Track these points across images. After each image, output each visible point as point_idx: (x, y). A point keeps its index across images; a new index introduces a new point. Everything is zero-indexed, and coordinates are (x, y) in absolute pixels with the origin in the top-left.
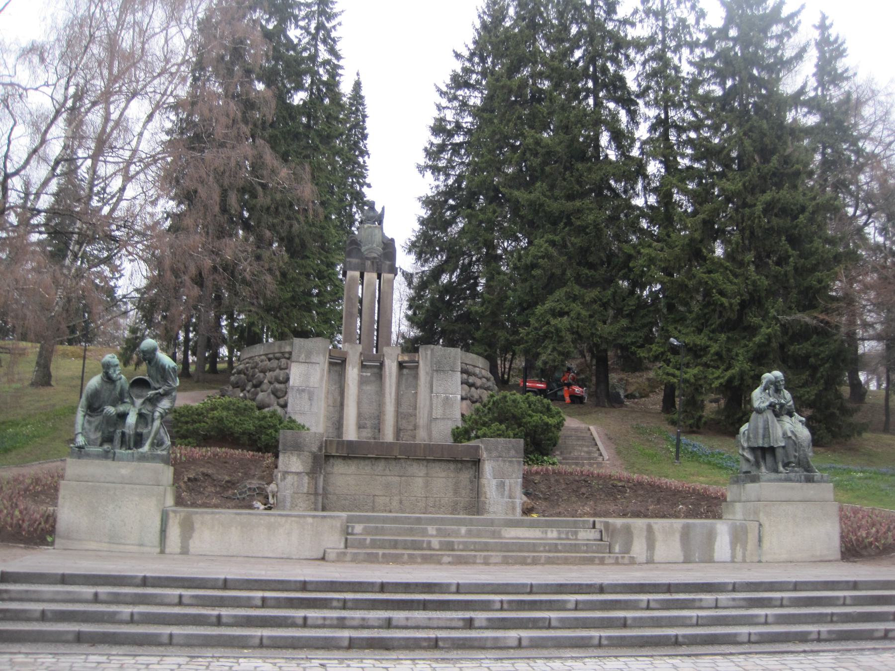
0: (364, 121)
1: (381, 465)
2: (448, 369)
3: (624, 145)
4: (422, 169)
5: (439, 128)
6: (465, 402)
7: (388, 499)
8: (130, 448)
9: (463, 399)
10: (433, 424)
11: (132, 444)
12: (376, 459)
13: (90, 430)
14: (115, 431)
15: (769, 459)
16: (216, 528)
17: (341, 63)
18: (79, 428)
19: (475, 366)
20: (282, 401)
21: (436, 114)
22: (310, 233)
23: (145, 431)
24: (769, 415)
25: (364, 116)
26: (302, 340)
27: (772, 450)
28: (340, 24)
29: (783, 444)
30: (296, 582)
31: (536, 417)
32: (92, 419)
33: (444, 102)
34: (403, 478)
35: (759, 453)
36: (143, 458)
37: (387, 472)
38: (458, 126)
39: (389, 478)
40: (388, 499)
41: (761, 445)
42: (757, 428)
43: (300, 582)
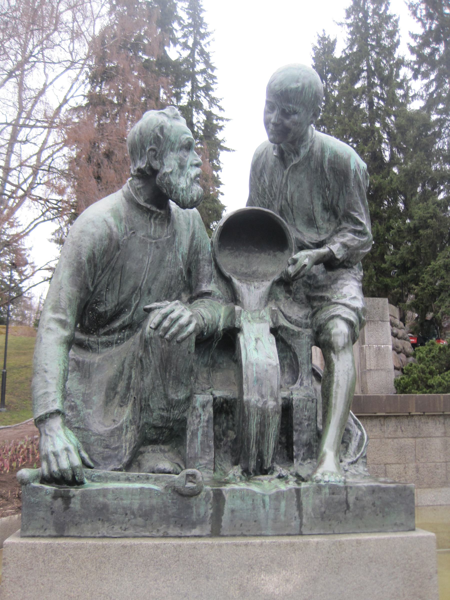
1: (391, 425)
2: (377, 319)
7: (402, 467)
10: (368, 375)
12: (385, 417)
17: (214, 74)
22: (206, 208)
28: (213, 40)
34: (418, 440)
37: (399, 433)
39: (402, 441)
40: (402, 467)
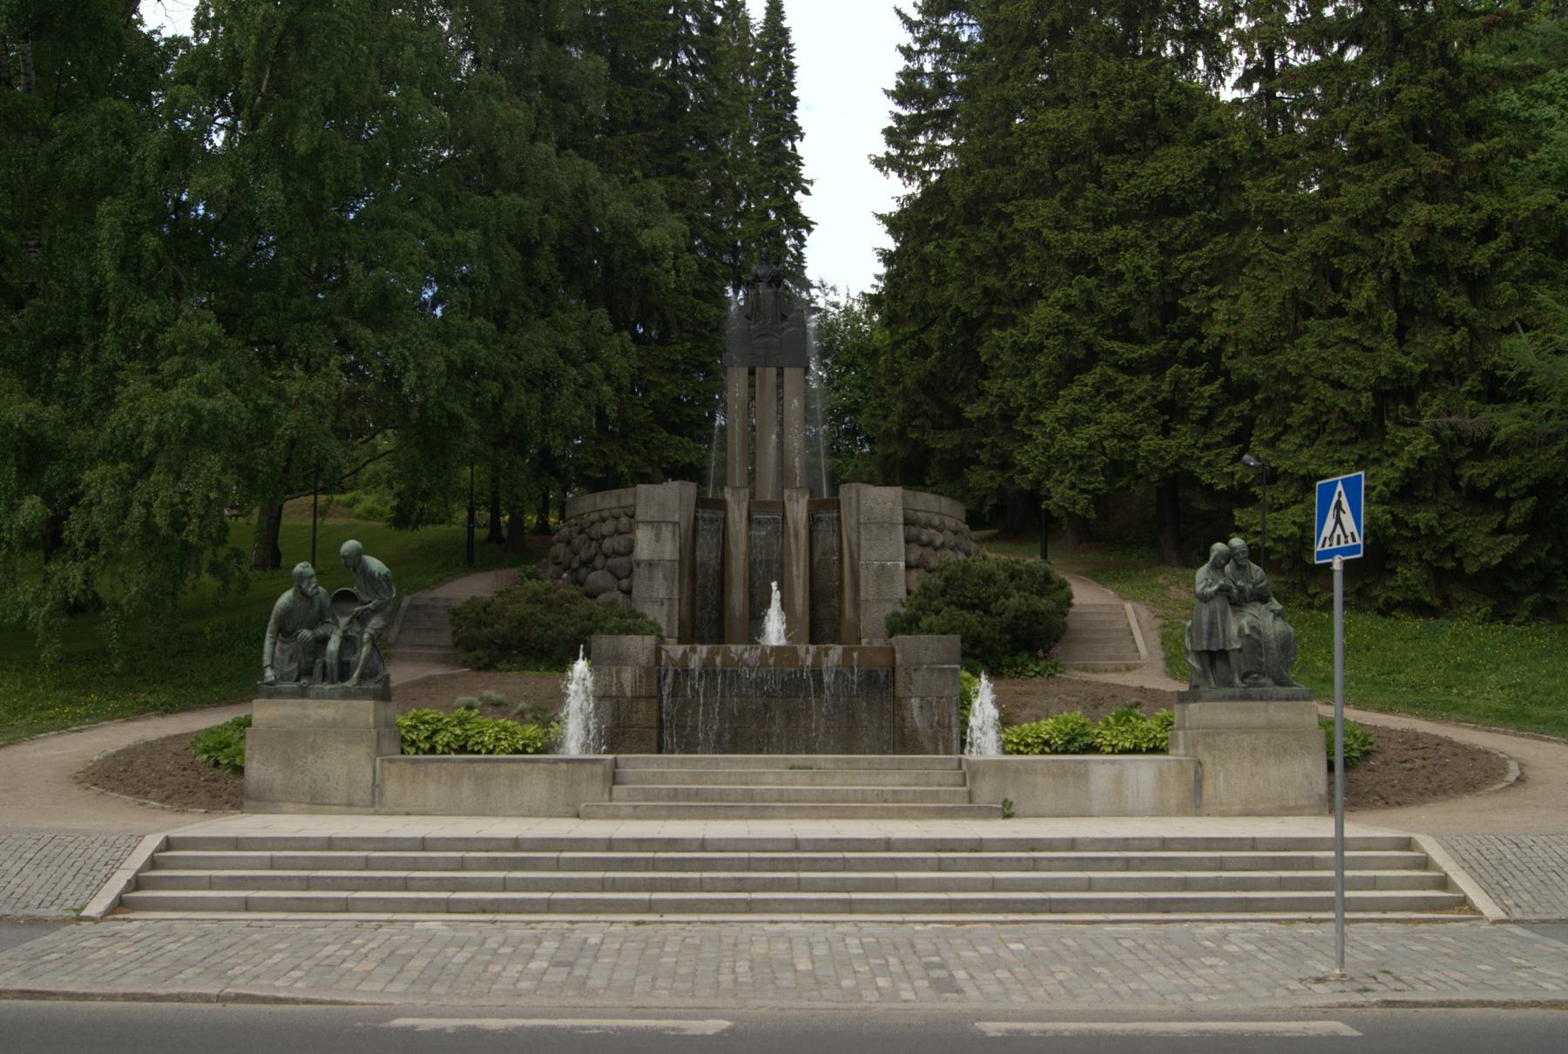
0: (791, 76)
4: (879, 163)
5: (903, 94)
6: (914, 574)
8: (333, 683)
9: (908, 567)
11: (335, 678)
13: (283, 661)
14: (314, 661)
15: (1219, 665)
18: (267, 660)
19: (916, 510)
20: (624, 583)
21: (901, 63)
23: (353, 659)
24: (1218, 604)
25: (791, 68)
26: (650, 486)
27: (1223, 654)
29: (1238, 646)
30: (507, 839)
32: (286, 646)
35: (1205, 658)
36: (347, 695)
41: (1205, 648)
42: (1200, 623)
43: (512, 839)
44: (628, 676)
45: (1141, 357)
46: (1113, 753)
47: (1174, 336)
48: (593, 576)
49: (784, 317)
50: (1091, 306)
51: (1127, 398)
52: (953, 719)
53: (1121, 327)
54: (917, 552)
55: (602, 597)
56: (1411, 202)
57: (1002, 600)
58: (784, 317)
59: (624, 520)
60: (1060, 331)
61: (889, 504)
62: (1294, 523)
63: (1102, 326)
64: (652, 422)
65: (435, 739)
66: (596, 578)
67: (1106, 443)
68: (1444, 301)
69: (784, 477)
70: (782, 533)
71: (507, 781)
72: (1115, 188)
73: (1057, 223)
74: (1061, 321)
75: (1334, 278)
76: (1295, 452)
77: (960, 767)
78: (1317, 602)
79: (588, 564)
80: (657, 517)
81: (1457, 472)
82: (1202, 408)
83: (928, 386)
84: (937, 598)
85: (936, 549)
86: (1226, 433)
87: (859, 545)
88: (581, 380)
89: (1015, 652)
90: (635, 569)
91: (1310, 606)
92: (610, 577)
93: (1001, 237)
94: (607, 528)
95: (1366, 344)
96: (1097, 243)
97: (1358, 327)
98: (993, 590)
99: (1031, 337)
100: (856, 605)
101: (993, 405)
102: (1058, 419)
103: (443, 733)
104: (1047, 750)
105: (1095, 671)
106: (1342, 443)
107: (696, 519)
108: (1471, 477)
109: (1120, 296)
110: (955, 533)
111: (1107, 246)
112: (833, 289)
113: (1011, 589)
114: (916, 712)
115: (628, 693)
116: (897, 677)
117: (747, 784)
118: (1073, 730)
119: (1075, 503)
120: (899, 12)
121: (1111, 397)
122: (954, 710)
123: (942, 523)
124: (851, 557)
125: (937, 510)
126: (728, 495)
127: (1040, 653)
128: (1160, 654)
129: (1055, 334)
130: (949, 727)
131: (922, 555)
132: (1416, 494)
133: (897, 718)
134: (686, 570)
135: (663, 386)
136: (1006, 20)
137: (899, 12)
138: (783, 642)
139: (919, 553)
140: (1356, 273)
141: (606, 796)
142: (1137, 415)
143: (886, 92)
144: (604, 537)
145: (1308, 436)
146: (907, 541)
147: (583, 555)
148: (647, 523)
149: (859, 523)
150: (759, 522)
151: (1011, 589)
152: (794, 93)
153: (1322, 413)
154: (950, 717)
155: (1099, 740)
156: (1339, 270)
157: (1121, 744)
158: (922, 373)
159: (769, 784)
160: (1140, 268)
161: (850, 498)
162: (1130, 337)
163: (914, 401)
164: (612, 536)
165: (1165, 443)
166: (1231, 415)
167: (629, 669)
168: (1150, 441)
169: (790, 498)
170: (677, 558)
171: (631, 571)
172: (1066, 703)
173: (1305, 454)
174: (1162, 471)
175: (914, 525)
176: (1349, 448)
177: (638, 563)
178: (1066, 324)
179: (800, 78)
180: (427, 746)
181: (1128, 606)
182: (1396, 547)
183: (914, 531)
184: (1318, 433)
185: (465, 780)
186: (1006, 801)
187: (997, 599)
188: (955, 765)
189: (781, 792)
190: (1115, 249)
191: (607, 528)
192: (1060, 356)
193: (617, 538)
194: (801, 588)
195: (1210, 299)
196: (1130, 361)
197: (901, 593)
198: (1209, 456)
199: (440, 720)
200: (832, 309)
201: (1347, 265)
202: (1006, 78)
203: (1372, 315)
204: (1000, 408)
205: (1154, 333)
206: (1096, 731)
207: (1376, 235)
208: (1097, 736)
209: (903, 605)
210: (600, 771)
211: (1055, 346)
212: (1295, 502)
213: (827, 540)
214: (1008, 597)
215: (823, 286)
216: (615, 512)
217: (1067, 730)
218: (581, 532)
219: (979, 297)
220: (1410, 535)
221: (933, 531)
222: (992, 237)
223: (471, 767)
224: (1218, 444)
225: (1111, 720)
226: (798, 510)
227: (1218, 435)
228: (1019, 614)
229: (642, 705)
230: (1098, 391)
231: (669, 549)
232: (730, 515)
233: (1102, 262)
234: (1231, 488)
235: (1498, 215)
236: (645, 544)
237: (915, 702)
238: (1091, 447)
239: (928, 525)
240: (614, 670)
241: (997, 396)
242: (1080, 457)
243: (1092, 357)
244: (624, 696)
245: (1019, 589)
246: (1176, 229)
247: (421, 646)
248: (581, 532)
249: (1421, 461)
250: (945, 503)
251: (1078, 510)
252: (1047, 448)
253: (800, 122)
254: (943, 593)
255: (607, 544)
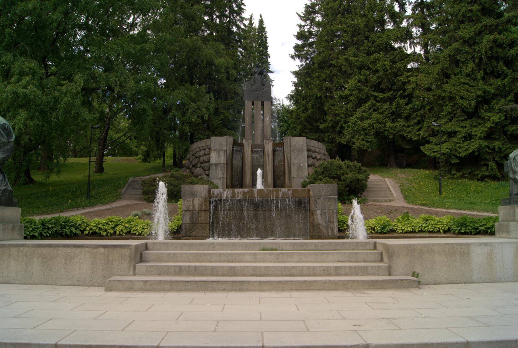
0: (266, 40)
3: (397, 21)
4: (292, 57)
5: (300, 36)
6: (310, 168)
9: (309, 166)
16: (21, 259)
19: (311, 146)
20: (207, 172)
25: (266, 38)
31: (350, 175)
33: (303, 23)
38: (310, 33)
44: (197, 202)
45: (384, 97)
46: (402, 233)
47: (395, 90)
48: (196, 170)
49: (264, 85)
50: (367, 81)
51: (380, 110)
52: (335, 219)
53: (377, 87)
54: (311, 161)
55: (199, 177)
56: (485, 35)
57: (345, 175)
58: (264, 85)
59: (207, 150)
60: (357, 89)
61: (301, 143)
62: (447, 148)
63: (371, 87)
64: (222, 126)
65: (116, 228)
66: (197, 171)
67: (374, 125)
68: (501, 67)
69: (264, 137)
70: (263, 155)
71: (63, 260)
72: (374, 42)
73: (354, 55)
74: (357, 85)
75: (457, 63)
76: (444, 124)
77: (375, 248)
78: (455, 177)
79: (195, 166)
80: (218, 148)
81: (505, 129)
82: (407, 113)
83: (309, 120)
84: (320, 175)
85: (318, 160)
86: (415, 121)
87: (291, 158)
88: (196, 107)
89: (349, 195)
90: (210, 167)
91: (452, 178)
92: (202, 170)
93: (331, 72)
94: (201, 153)
95: (471, 84)
96: (368, 60)
97: (468, 79)
98: (342, 172)
99: (347, 92)
100: (290, 179)
101: (329, 123)
102: (357, 118)
103: (120, 226)
104: (373, 232)
105: (378, 202)
106: (462, 121)
107: (233, 150)
108: (513, 131)
109: (377, 77)
110: (324, 155)
111: (372, 61)
112: (279, 100)
113: (348, 171)
114: (319, 216)
115: (197, 209)
116: (311, 202)
117: (232, 262)
118: (384, 223)
119: (364, 146)
120: (298, 14)
121: (375, 110)
122: (335, 215)
123: (320, 151)
124: (288, 162)
125: (318, 147)
126: (244, 142)
127: (359, 195)
128: (401, 196)
129: (355, 90)
130: (333, 223)
131: (313, 162)
132: (492, 137)
133: (311, 219)
134: (229, 168)
135: (225, 114)
136: (331, 8)
137: (298, 14)
138: (262, 187)
139: (312, 161)
140: (466, 61)
141: (131, 272)
142: (384, 116)
143: (294, 35)
144: (200, 156)
145: (449, 119)
146: (308, 157)
147: (193, 163)
148: (215, 150)
149: (290, 150)
150: (255, 151)
151: (348, 171)
152: (267, 45)
153: (454, 110)
154: (333, 218)
155: (396, 227)
156: (459, 60)
157: (406, 229)
158: (306, 116)
159: (247, 262)
160: (385, 65)
161: (287, 142)
162: (382, 91)
163: (304, 124)
164: (203, 156)
165: (395, 125)
166: (417, 115)
167: (198, 199)
168: (389, 124)
169: (266, 143)
170: (225, 162)
171: (209, 168)
172: (377, 213)
173: (449, 125)
174: (394, 135)
175: (310, 151)
176: (465, 122)
177: (212, 165)
178: (359, 86)
179: (268, 40)
180: (112, 232)
181: (386, 179)
182: (485, 156)
183: (310, 153)
184: (452, 117)
185: (35, 259)
186: (414, 273)
187: (343, 175)
188: (372, 247)
189: (255, 268)
190: (374, 62)
191: (201, 153)
192: (357, 97)
193: (205, 156)
194: (270, 174)
195: (408, 77)
196: (381, 99)
197: (306, 174)
198: (409, 129)
199: (120, 220)
200: (278, 105)
201: (461, 58)
202: (332, 25)
203: (473, 74)
204: (332, 124)
205: (390, 89)
206: (394, 224)
207: (472, 47)
208: (394, 226)
209: (308, 178)
210: (127, 254)
211: (356, 93)
212: (446, 141)
213: (279, 158)
214: (347, 174)
215: (276, 99)
216: (204, 147)
217: (381, 224)
218: (193, 155)
219: (324, 91)
220: (490, 152)
221: (317, 154)
222: (328, 72)
223: (39, 250)
224: (412, 125)
225: (400, 219)
226: (269, 147)
227: (412, 122)
228: (352, 180)
229: (203, 214)
230: (370, 109)
231: (223, 160)
232: (245, 149)
233: (370, 66)
234: (419, 139)
235: (515, 40)
236: (214, 158)
237: (319, 212)
238: (369, 127)
239: (315, 152)
240: (191, 199)
241: (330, 120)
242: (366, 129)
243: (368, 98)
244: (196, 210)
245: (351, 171)
246: (395, 54)
247: (133, 194)
248: (193, 155)
249: (497, 124)
250: (320, 145)
251: (365, 148)
252: (353, 128)
253: (269, 53)
254: (323, 173)
255: (202, 159)
